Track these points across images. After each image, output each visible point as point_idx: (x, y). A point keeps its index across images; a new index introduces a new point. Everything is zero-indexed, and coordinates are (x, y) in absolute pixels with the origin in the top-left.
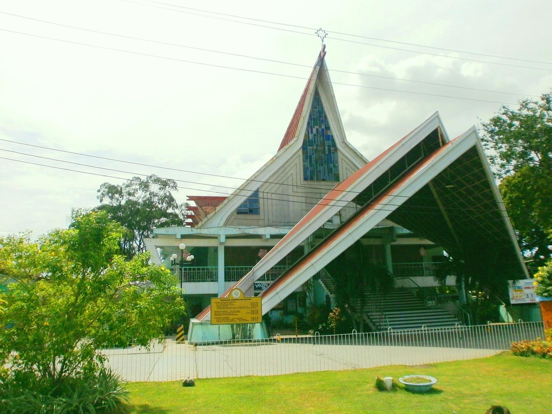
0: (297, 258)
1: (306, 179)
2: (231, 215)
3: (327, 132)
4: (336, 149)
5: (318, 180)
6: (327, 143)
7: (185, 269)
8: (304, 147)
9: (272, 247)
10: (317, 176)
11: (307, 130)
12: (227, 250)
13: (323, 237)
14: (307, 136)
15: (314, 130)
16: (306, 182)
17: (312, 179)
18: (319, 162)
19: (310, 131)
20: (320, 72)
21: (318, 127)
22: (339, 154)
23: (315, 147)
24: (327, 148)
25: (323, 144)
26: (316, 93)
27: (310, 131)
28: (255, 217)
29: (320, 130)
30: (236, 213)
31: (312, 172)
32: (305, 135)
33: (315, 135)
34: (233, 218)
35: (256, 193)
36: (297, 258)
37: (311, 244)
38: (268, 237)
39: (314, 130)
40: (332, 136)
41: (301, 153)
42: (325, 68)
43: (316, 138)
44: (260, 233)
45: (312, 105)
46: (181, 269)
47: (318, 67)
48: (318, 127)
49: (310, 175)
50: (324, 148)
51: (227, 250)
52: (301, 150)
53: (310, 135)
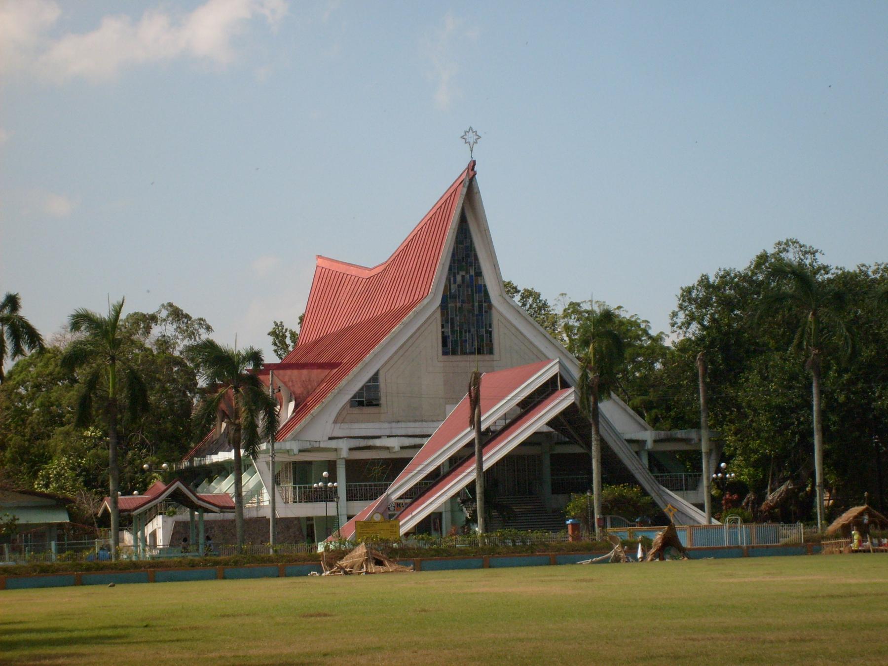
0: (436, 478)
1: (445, 353)
2: (343, 408)
4: (490, 306)
5: (463, 353)
6: (476, 297)
7: (300, 488)
8: (444, 306)
9: (411, 459)
10: (462, 349)
11: (448, 279)
14: (447, 288)
15: (459, 278)
16: (446, 357)
17: (454, 353)
19: (452, 279)
20: (472, 166)
22: (494, 312)
23: (459, 305)
24: (476, 304)
25: (471, 299)
26: (463, 220)
27: (452, 279)
29: (468, 277)
31: (455, 343)
32: (446, 286)
33: (459, 286)
35: (375, 378)
36: (436, 478)
37: (446, 469)
39: (459, 278)
40: (485, 286)
41: (438, 315)
42: (475, 190)
44: (388, 445)
45: (457, 238)
48: (463, 273)
49: (451, 346)
50: (473, 306)
52: (439, 311)
53: (453, 286)
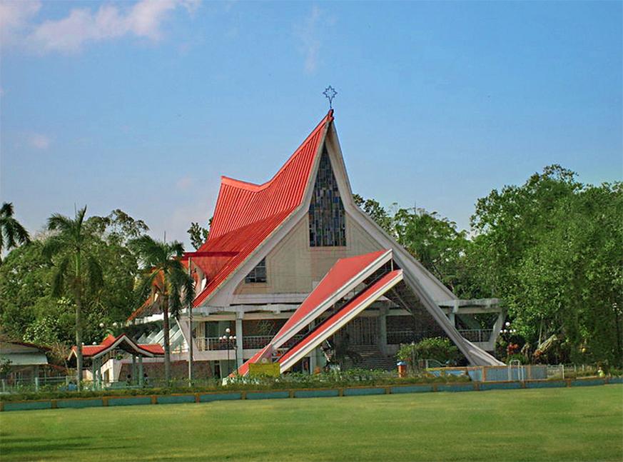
0: (306, 333)
2: (240, 283)
3: (334, 194)
4: (344, 212)
8: (311, 212)
11: (314, 193)
12: (244, 323)
13: (343, 305)
14: (314, 199)
15: (322, 192)
17: (318, 245)
18: (326, 227)
21: (325, 189)
28: (262, 285)
30: (244, 281)
32: (312, 198)
34: (240, 288)
36: (306, 333)
38: (207, 314)
39: (322, 192)
40: (340, 198)
41: (307, 218)
43: (323, 200)
46: (206, 340)
47: (322, 139)
48: (325, 189)
49: (315, 241)
51: (244, 323)
52: (308, 215)
53: (317, 198)
